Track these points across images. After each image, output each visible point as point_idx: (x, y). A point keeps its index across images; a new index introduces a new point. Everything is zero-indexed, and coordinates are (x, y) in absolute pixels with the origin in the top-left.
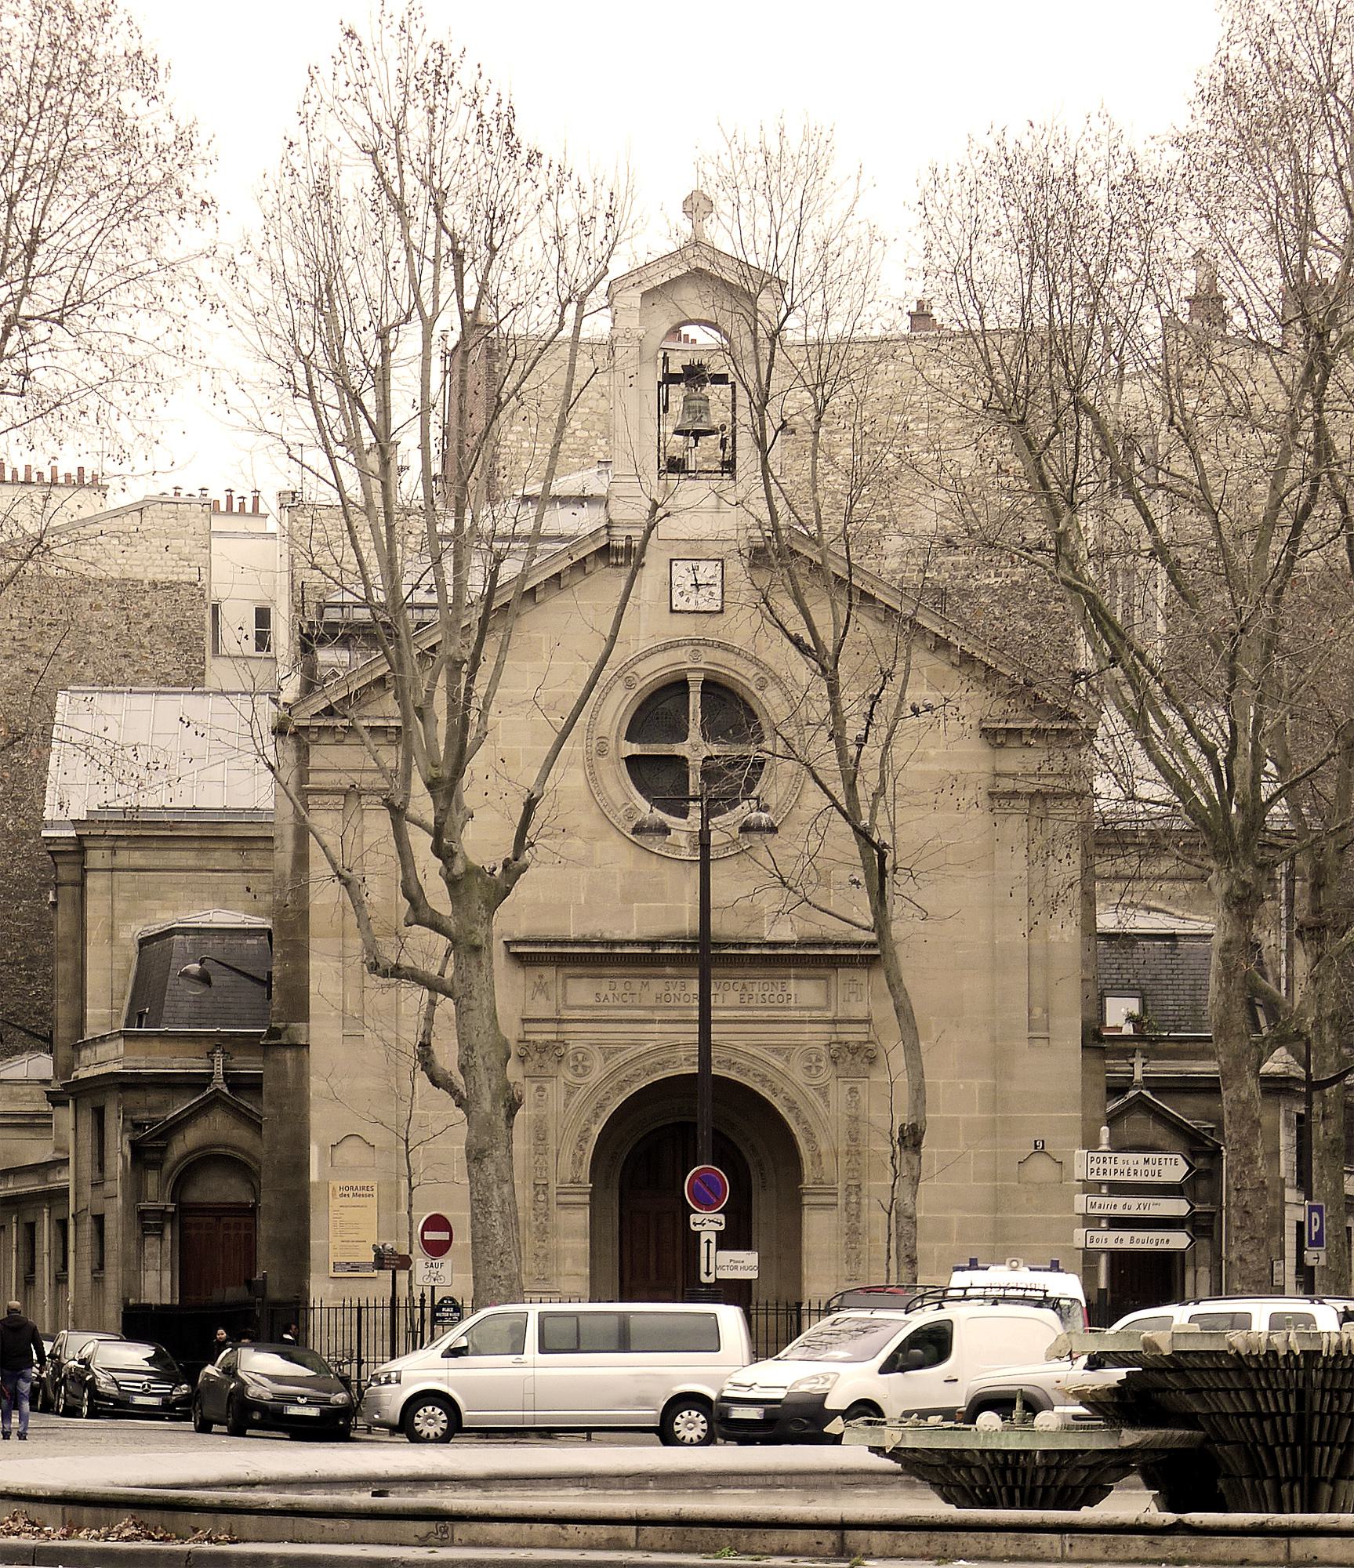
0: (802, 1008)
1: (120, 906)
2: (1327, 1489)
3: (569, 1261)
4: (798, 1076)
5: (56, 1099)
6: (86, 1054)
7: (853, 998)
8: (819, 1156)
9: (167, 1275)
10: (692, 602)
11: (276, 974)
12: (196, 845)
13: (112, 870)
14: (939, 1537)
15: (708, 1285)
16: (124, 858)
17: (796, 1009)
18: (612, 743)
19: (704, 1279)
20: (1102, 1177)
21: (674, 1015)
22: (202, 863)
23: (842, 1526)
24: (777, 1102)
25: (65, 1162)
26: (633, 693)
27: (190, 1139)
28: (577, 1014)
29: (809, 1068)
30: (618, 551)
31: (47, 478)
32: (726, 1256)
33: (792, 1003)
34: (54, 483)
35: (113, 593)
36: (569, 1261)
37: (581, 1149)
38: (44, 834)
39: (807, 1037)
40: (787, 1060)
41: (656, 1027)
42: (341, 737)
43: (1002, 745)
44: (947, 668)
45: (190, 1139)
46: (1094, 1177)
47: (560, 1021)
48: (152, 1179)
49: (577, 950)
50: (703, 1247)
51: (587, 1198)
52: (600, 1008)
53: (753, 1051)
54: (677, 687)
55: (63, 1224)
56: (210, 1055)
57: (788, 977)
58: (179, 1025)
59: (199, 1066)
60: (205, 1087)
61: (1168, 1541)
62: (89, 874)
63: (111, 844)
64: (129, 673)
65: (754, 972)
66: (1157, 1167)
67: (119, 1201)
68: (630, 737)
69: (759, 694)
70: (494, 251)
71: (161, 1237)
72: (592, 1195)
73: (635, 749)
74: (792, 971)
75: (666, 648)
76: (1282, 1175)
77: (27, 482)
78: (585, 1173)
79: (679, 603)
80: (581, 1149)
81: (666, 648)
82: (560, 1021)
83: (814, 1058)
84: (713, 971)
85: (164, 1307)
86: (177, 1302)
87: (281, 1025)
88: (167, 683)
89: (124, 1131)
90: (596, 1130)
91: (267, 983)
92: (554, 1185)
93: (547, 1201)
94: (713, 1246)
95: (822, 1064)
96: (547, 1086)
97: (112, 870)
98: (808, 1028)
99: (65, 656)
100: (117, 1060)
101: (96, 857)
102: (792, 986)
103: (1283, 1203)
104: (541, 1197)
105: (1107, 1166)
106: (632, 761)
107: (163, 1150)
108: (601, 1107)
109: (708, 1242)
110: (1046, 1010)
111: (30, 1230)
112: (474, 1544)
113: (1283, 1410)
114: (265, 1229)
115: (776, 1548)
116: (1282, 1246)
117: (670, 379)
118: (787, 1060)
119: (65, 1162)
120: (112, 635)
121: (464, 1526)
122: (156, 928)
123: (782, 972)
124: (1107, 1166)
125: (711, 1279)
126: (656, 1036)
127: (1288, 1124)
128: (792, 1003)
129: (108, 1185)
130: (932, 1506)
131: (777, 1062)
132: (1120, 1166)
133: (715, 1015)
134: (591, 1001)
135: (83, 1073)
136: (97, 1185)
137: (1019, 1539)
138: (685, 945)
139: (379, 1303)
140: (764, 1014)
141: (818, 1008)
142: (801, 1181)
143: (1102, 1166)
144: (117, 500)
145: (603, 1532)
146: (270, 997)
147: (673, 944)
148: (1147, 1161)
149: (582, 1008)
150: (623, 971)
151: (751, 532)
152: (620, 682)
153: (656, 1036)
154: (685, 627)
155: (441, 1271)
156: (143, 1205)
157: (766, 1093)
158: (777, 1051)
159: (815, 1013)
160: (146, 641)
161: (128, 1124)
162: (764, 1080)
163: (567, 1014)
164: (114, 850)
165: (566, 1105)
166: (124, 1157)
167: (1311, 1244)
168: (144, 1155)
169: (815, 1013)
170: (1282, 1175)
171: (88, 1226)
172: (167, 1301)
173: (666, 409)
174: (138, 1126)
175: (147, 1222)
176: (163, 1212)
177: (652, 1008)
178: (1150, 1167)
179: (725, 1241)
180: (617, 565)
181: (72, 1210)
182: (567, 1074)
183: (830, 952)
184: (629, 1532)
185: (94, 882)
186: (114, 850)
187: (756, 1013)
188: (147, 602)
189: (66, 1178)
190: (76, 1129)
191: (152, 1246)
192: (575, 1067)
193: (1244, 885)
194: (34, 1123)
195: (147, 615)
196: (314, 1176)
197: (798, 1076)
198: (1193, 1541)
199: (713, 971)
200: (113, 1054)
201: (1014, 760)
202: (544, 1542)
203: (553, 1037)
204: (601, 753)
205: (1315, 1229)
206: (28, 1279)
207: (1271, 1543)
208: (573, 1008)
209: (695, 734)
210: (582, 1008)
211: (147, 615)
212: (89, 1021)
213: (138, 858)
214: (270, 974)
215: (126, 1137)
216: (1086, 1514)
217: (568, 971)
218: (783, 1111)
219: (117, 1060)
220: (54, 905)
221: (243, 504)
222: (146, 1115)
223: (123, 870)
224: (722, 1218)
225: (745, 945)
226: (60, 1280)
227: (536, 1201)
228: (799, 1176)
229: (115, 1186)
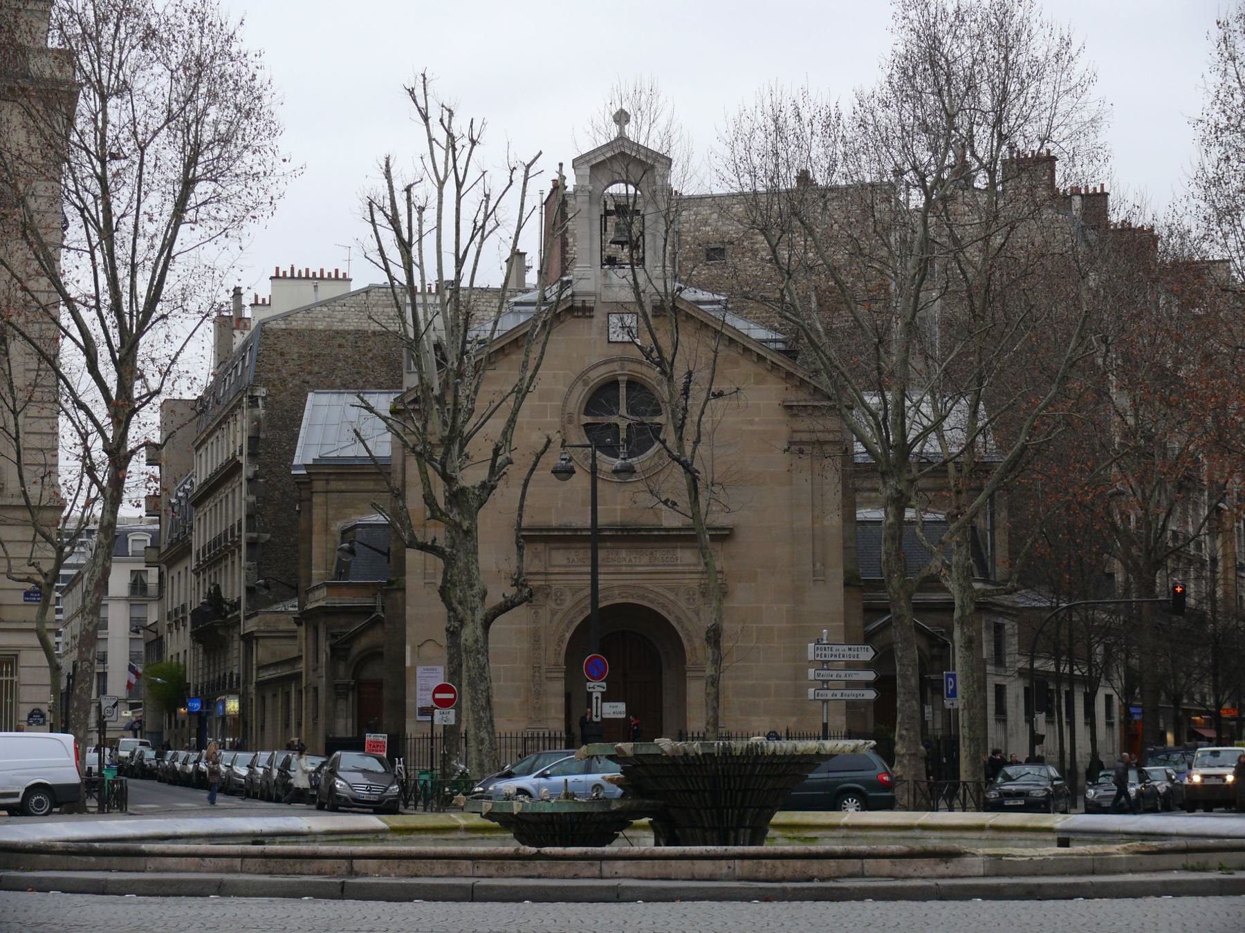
0: (684, 565)
1: (331, 512)
2: (732, 834)
3: (553, 711)
4: (683, 604)
5: (298, 622)
6: (311, 596)
8: (695, 649)
9: (350, 721)
10: (621, 336)
11: (392, 549)
12: (373, 477)
13: (326, 492)
14: (410, 863)
15: (597, 723)
16: (334, 485)
18: (576, 416)
19: (595, 719)
20: (823, 659)
21: (612, 569)
22: (378, 487)
23: (351, 857)
24: (671, 619)
25: (300, 657)
26: (587, 389)
27: (364, 642)
28: (557, 570)
30: (578, 309)
31: (304, 275)
32: (606, 706)
33: (679, 562)
34: (322, 278)
35: (351, 338)
36: (553, 711)
37: (560, 646)
38: (293, 472)
40: (676, 594)
42: (810, 412)
43: (795, 415)
44: (764, 372)
45: (364, 642)
46: (819, 658)
47: (547, 574)
48: (342, 668)
49: (556, 533)
50: (594, 701)
51: (563, 675)
52: (569, 566)
53: (656, 589)
54: (611, 385)
55: (300, 692)
56: (374, 595)
57: (677, 548)
58: (361, 579)
59: (367, 602)
60: (371, 614)
61: (531, 864)
62: (314, 495)
63: (325, 477)
64: (360, 383)
65: (656, 545)
66: (856, 653)
67: (324, 679)
68: (587, 413)
69: (659, 388)
70: (473, 142)
71: (347, 699)
72: (566, 673)
73: (589, 420)
74: (679, 544)
75: (605, 363)
76: (985, 657)
77: (307, 277)
78: (562, 660)
79: (613, 338)
80: (560, 646)
81: (605, 363)
82: (547, 574)
84: (599, 545)
85: (349, 739)
86: (356, 735)
87: (393, 579)
88: (381, 388)
89: (326, 640)
90: (568, 636)
91: (388, 554)
92: (544, 667)
93: (540, 677)
94: (599, 701)
96: (540, 611)
97: (326, 492)
98: (688, 576)
99: (324, 373)
100: (323, 599)
101: (319, 485)
102: (679, 553)
103: (985, 674)
104: (537, 674)
105: (827, 653)
106: (586, 425)
107: (349, 649)
108: (571, 622)
109: (597, 698)
110: (823, 565)
111: (288, 694)
112: (157, 870)
113: (702, 788)
114: (386, 693)
115: (316, 871)
116: (985, 699)
117: (608, 213)
119: (300, 657)
120: (350, 361)
121: (152, 859)
122: (349, 525)
123: (673, 544)
124: (827, 653)
125: (599, 719)
127: (987, 627)
128: (679, 562)
129: (319, 670)
130: (510, 845)
131: (671, 596)
132: (834, 653)
133: (600, 570)
134: (565, 562)
135: (309, 607)
136: (315, 670)
137: (448, 863)
138: (617, 530)
139: (558, 735)
140: (663, 569)
141: (694, 565)
142: (685, 664)
143: (824, 652)
144: (355, 286)
145: (224, 862)
146: (389, 562)
147: (610, 530)
148: (850, 649)
149: (559, 566)
150: (564, 545)
151: (653, 297)
152: (580, 383)
154: (616, 351)
155: (449, 716)
156: (337, 681)
157: (664, 613)
158: (671, 589)
159: (692, 568)
160: (369, 364)
161: (329, 636)
162: (664, 606)
163: (550, 570)
164: (327, 481)
165: (551, 622)
166: (327, 654)
167: (948, 696)
168: (338, 652)
169: (692, 568)
170: (985, 657)
171: (311, 693)
172: (350, 735)
173: (606, 230)
174: (334, 636)
175: (338, 691)
176: (348, 685)
178: (852, 653)
179: (607, 697)
180: (578, 317)
181: (304, 685)
182: (551, 604)
183: (545, 533)
184: (237, 862)
185: (317, 499)
186: (327, 481)
187: (659, 568)
188: (370, 343)
189: (302, 666)
190: (306, 639)
191: (341, 705)
192: (556, 600)
193: (900, 492)
194: (292, 636)
195: (370, 350)
196: (408, 663)
197: (683, 604)
198: (545, 863)
199: (599, 545)
200: (322, 596)
201: (804, 423)
202: (193, 869)
203: (543, 583)
204: (570, 422)
205: (951, 687)
206: (287, 725)
207: (592, 865)
208: (555, 566)
209: (623, 410)
210: (559, 566)
211: (370, 350)
212: (313, 577)
213: (341, 485)
214: (389, 549)
215: (328, 643)
216: (608, 849)
217: (552, 545)
218: (674, 624)
219: (323, 599)
220: (299, 512)
221: (430, 289)
222: (339, 630)
223: (333, 492)
224: (604, 684)
225: (640, 530)
226: (299, 724)
227: (534, 676)
228: (684, 662)
229: (322, 671)
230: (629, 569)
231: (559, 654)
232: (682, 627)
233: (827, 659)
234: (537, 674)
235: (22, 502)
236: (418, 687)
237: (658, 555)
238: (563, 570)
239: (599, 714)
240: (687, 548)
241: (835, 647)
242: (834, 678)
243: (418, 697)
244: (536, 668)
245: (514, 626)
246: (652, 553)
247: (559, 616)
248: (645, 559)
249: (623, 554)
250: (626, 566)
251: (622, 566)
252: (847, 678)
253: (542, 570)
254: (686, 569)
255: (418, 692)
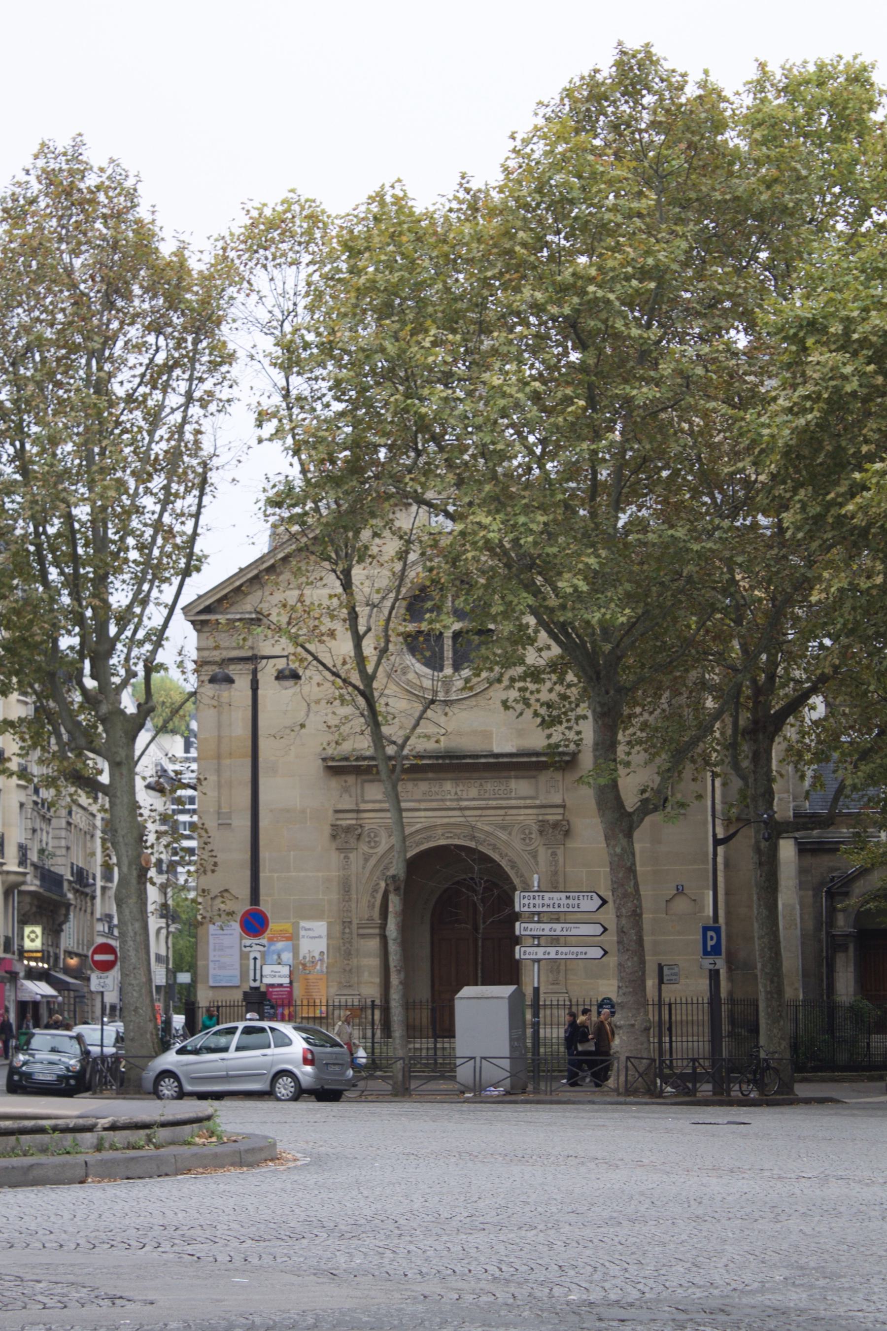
3: (366, 974)
7: (552, 790)
17: (516, 799)
21: (434, 805)
28: (370, 806)
29: (524, 839)
33: (513, 795)
36: (366, 974)
39: (522, 818)
40: (510, 834)
41: (422, 814)
47: (358, 811)
65: (486, 775)
66: (576, 902)
73: (411, 627)
74: (513, 773)
83: (527, 831)
93: (351, 933)
95: (533, 836)
96: (351, 855)
98: (522, 811)
102: (513, 784)
104: (347, 930)
105: (541, 902)
118: (510, 834)
123: (441, 775)
126: (423, 820)
128: (513, 795)
132: (546, 902)
140: (493, 803)
143: (532, 902)
147: (430, 757)
148: (568, 898)
153: (423, 820)
158: (503, 828)
159: (528, 802)
163: (363, 806)
165: (364, 868)
169: (528, 802)
177: (419, 801)
178: (571, 902)
182: (364, 848)
183: (534, 759)
192: (369, 842)
197: (517, 844)
203: (354, 822)
218: (507, 869)
227: (344, 933)
230: (454, 804)
231: (373, 906)
232: (517, 873)
233: (537, 909)
234: (347, 930)
235: (170, 726)
236: (211, 947)
237: (489, 786)
238: (377, 806)
239: (258, 977)
240: (523, 778)
241: (547, 895)
242: (547, 932)
243: (211, 958)
244: (346, 924)
245: (320, 874)
246: (481, 785)
247: (372, 862)
248: (473, 792)
249: (448, 786)
250: (451, 800)
251: (446, 800)
252: (552, 933)
253: (353, 807)
254: (521, 803)
255: (211, 954)
